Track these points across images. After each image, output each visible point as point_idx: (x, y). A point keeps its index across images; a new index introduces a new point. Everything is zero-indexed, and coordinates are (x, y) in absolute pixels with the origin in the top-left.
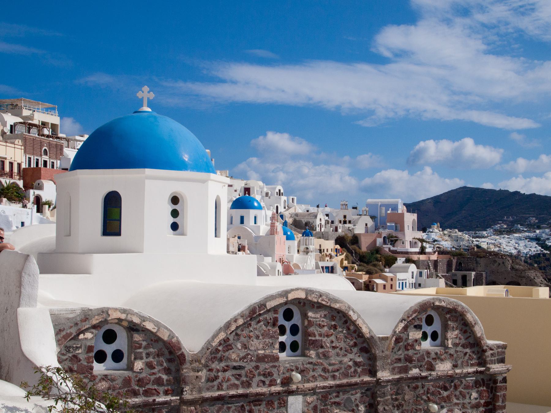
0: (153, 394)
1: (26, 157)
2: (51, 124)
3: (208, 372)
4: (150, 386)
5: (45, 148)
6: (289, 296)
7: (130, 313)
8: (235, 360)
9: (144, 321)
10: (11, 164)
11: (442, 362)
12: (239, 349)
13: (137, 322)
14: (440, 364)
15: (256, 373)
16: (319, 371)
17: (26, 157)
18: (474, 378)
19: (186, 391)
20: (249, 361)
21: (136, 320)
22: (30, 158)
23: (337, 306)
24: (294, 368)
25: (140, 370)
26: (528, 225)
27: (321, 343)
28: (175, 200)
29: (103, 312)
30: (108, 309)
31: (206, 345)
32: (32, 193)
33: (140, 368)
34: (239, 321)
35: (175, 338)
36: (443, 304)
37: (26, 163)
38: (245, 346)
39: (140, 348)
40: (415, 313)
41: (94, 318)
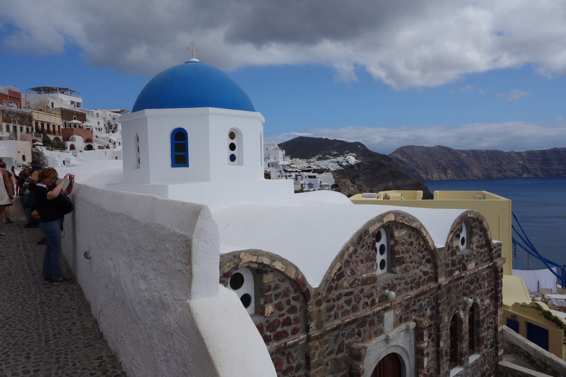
0: (283, 338)
1: (63, 122)
2: (77, 102)
3: (326, 303)
4: (279, 329)
5: (74, 116)
6: (384, 220)
7: (260, 255)
8: (346, 288)
9: (274, 261)
10: (54, 126)
11: (499, 269)
12: (349, 276)
13: (267, 264)
14: (469, 264)
15: (362, 295)
16: (403, 285)
17: (63, 122)
18: (486, 272)
19: (311, 327)
20: (356, 286)
21: (266, 261)
22: (65, 123)
23: (414, 225)
24: (386, 286)
25: (270, 314)
26: (333, 155)
27: (403, 259)
28: (232, 135)
29: (235, 257)
30: (240, 252)
31: (325, 277)
32: (69, 144)
33: (270, 313)
34: (350, 249)
35: (300, 275)
36: (472, 215)
37: (63, 126)
38: (353, 273)
39: (269, 290)
40: (458, 225)
41: (226, 265)
